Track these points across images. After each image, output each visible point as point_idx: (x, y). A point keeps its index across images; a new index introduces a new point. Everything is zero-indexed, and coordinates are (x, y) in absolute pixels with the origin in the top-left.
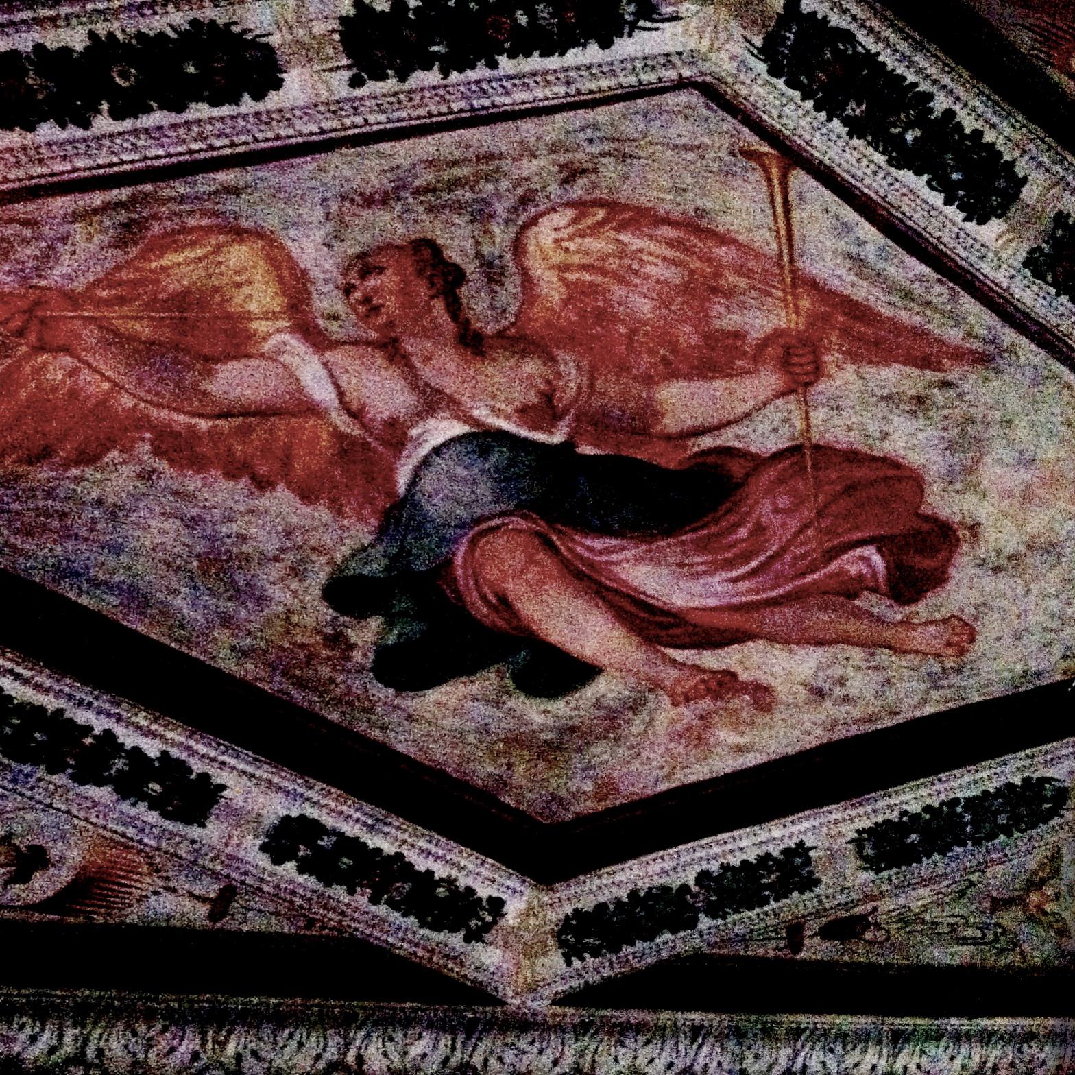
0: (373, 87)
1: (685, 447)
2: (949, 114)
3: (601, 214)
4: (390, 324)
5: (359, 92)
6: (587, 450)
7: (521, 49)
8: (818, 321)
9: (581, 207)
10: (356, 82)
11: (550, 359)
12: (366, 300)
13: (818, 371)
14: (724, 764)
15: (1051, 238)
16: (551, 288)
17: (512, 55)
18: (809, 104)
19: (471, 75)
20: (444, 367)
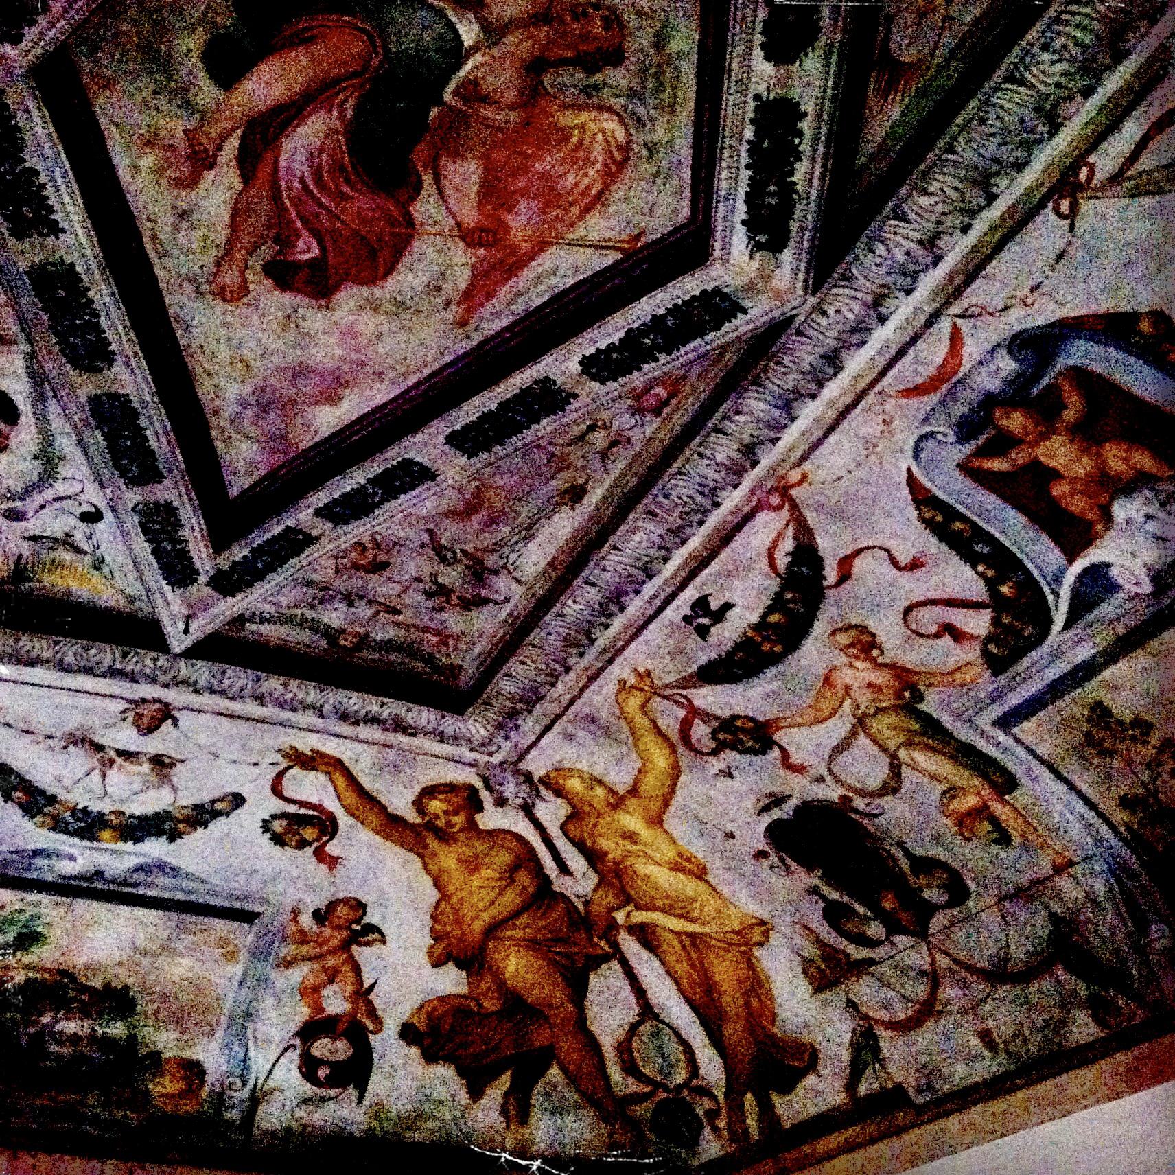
0: (751, 105)
1: (425, 167)
2: (656, 360)
3: (618, 156)
4: (562, 22)
5: (750, 98)
6: (434, 112)
7: (753, 182)
8: (513, 249)
9: (626, 148)
10: (757, 97)
11: (513, 107)
12: (585, 14)
13: (469, 245)
14: (121, 162)
15: (560, 391)
16: (567, 119)
17: (750, 178)
18: (680, 302)
19: (744, 155)
20: (517, 45)
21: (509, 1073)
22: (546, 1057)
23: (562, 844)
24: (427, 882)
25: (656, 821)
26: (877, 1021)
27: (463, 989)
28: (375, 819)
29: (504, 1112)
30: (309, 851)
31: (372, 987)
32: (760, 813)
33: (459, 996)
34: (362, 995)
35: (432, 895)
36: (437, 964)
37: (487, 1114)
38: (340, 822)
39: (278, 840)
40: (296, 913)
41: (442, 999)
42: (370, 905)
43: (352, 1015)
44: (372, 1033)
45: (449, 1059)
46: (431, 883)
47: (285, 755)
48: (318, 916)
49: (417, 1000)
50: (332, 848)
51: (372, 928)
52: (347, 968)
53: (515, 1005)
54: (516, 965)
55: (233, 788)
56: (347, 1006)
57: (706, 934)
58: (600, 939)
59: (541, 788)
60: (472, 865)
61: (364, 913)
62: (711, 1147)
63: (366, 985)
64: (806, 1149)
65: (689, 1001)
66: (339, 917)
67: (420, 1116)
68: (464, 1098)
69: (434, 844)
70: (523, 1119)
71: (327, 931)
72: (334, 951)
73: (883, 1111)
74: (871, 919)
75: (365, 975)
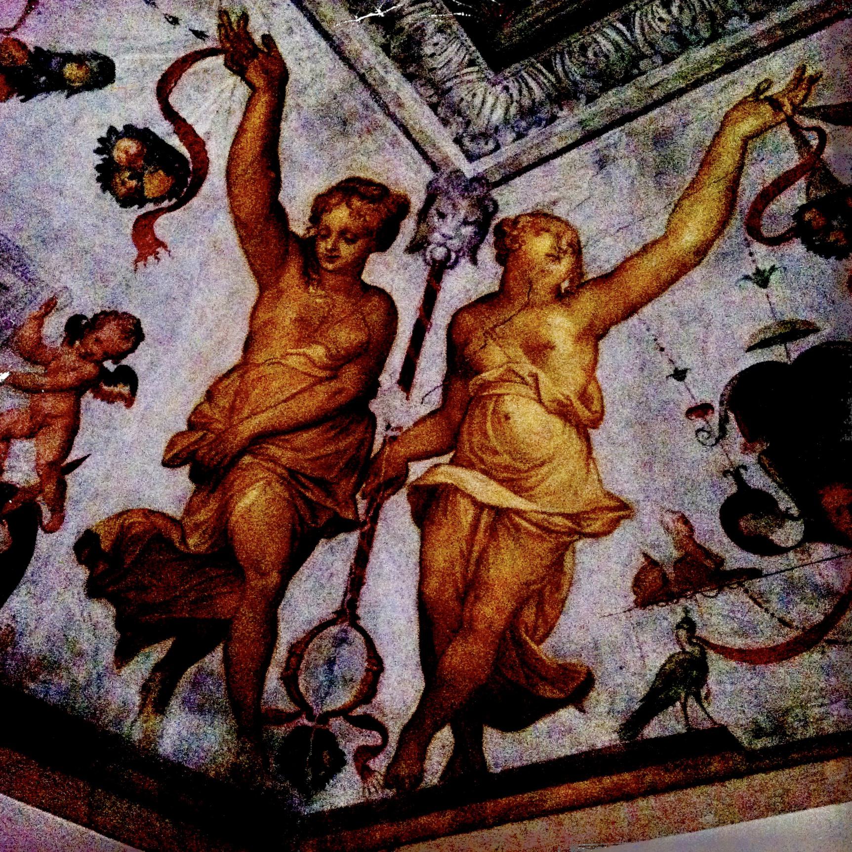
21: (169, 643)
22: (218, 632)
23: (435, 345)
24: (239, 333)
25: (593, 334)
26: (715, 648)
27: (174, 510)
28: (248, 203)
29: (145, 690)
30: (133, 214)
31: (78, 463)
32: (750, 349)
33: (164, 516)
34: (58, 470)
35: (233, 356)
36: (170, 463)
37: (126, 688)
38: (206, 188)
39: (107, 175)
40: (50, 306)
41: (148, 513)
42: (148, 339)
43: (32, 491)
44: (44, 529)
45: (114, 599)
46: (244, 335)
47: (224, 25)
48: (77, 328)
49: (114, 506)
50: (163, 227)
51: (129, 377)
52: (59, 424)
53: (224, 552)
54: (255, 500)
55: (104, 48)
56: (34, 480)
57: (519, 513)
58: (364, 497)
59: (490, 238)
60: (309, 329)
61: (132, 350)
62: (344, 792)
63: (73, 456)
64: (535, 795)
65: (424, 605)
66: (98, 341)
67: (51, 665)
68: (107, 655)
69: (291, 276)
70: (161, 707)
71: (70, 358)
72: (56, 390)
73: (676, 753)
74: (792, 518)
75: (79, 440)
